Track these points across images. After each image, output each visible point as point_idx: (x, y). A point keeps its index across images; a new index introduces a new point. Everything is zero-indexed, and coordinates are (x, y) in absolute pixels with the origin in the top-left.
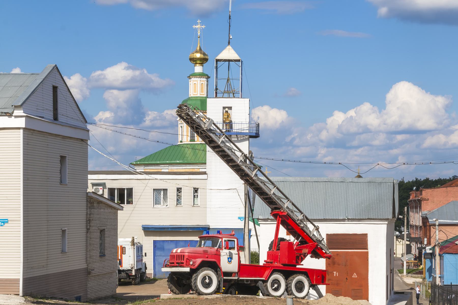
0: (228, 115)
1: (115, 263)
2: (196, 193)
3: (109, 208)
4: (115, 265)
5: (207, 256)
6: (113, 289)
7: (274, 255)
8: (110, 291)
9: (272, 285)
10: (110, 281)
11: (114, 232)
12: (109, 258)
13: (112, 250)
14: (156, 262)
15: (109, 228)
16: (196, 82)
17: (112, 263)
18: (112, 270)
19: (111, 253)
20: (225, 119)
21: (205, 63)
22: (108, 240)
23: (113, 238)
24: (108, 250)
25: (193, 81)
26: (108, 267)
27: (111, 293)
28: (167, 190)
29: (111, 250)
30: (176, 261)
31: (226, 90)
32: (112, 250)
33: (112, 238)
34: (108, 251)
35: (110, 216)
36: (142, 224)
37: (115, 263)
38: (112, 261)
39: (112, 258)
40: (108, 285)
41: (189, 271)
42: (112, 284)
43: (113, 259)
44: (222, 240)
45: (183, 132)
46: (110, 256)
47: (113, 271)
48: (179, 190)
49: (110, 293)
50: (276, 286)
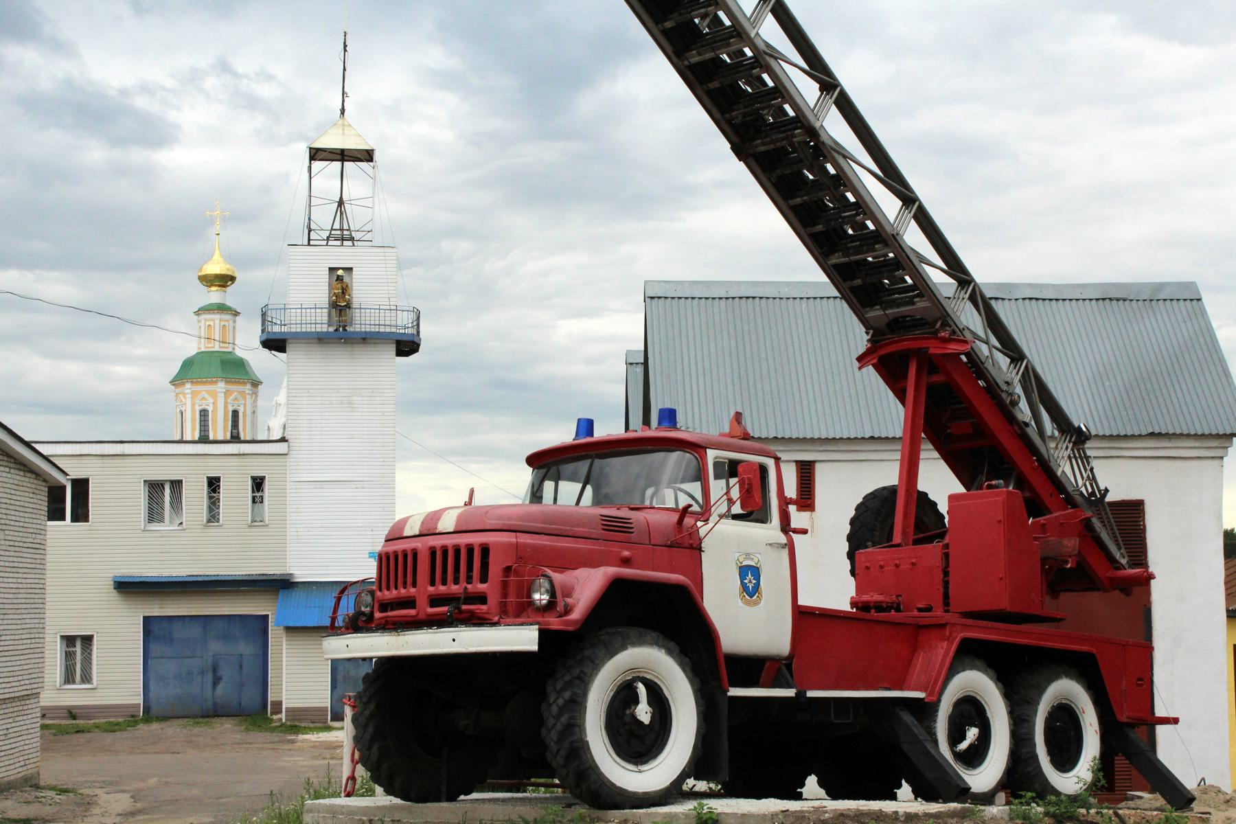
0: (344, 287)
1: (36, 666)
2: (258, 491)
3: (15, 469)
4: (37, 671)
5: (626, 553)
6: (26, 757)
7: (905, 567)
8: (18, 765)
9: (956, 736)
10: (15, 729)
11: (33, 556)
12: (15, 647)
13: (24, 616)
14: (152, 674)
15: (14, 538)
16: (212, 323)
17: (23, 662)
18: (25, 687)
19: (20, 627)
20: (336, 297)
21: (228, 286)
22: (10, 580)
23: (29, 576)
24: (11, 617)
25: (206, 320)
26: (11, 679)
27: (20, 769)
28: (180, 482)
29: (20, 617)
30: (431, 589)
31: (337, 226)
32: (24, 616)
33: (25, 576)
34: (9, 622)
35: (19, 498)
36: (112, 575)
37: (36, 666)
38: (26, 657)
39: (24, 647)
40: (12, 741)
41: (535, 648)
42: (25, 737)
43: (27, 651)
44: (703, 458)
45: (185, 421)
46: (17, 637)
47: (29, 692)
48: (213, 484)
49: (16, 771)
50: (972, 733)
